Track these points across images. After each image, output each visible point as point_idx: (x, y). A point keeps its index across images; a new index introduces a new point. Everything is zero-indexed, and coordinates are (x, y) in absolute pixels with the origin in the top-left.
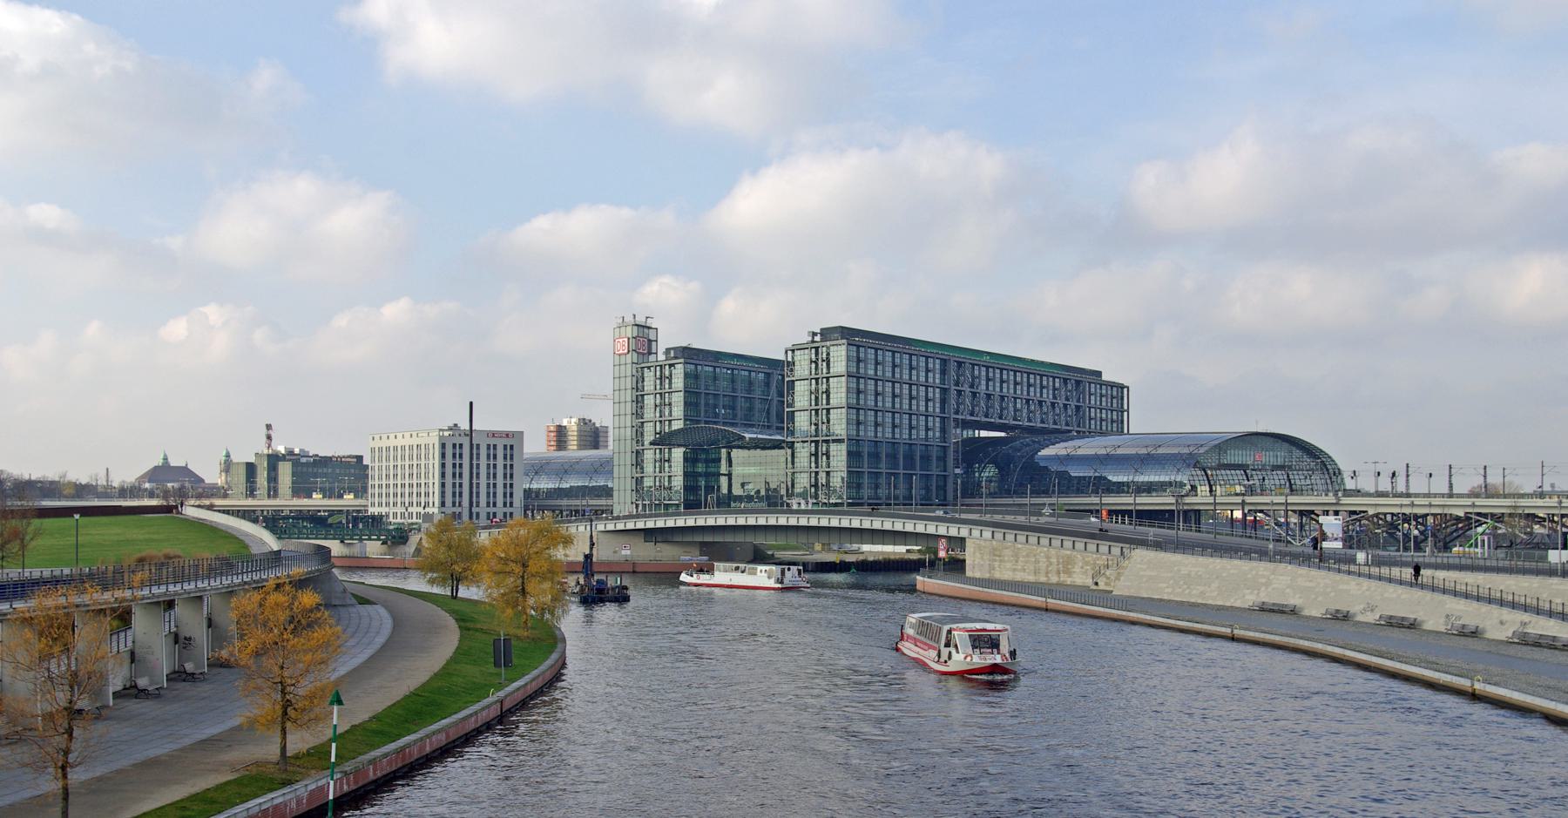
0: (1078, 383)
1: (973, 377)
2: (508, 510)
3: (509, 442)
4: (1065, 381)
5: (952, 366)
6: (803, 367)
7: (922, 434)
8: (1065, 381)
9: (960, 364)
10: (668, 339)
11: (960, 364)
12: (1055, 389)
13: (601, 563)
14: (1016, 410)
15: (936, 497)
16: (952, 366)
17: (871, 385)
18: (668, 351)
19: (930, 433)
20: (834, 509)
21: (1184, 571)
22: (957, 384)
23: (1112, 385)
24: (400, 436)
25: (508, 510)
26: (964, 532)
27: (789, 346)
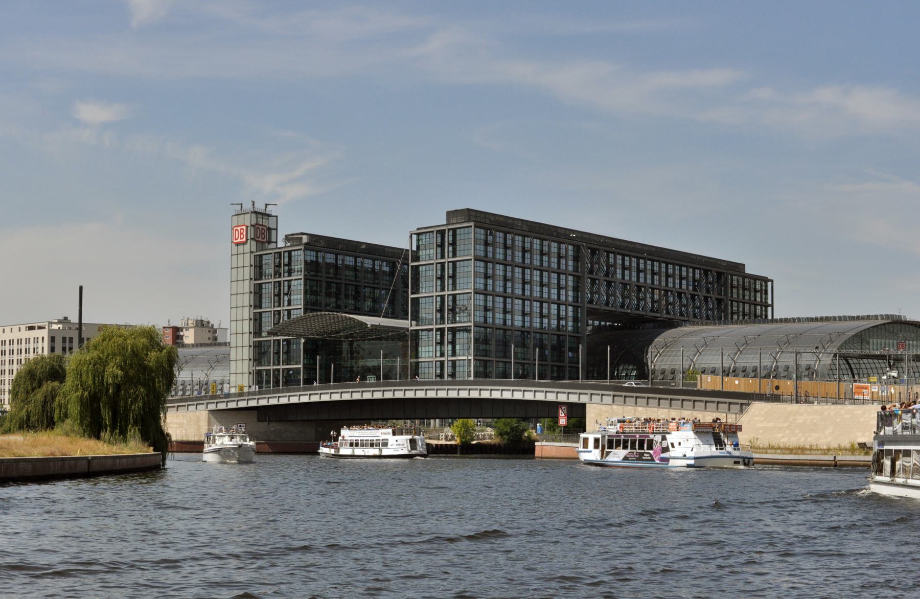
0: (719, 275)
1: (608, 266)
6: (429, 255)
8: (706, 272)
10: (287, 226)
12: (694, 280)
15: (558, 370)
17: (500, 270)
18: (288, 238)
19: (563, 323)
20: (290, 381)
21: (800, 420)
23: (755, 278)
24: (8, 329)
27: (414, 230)
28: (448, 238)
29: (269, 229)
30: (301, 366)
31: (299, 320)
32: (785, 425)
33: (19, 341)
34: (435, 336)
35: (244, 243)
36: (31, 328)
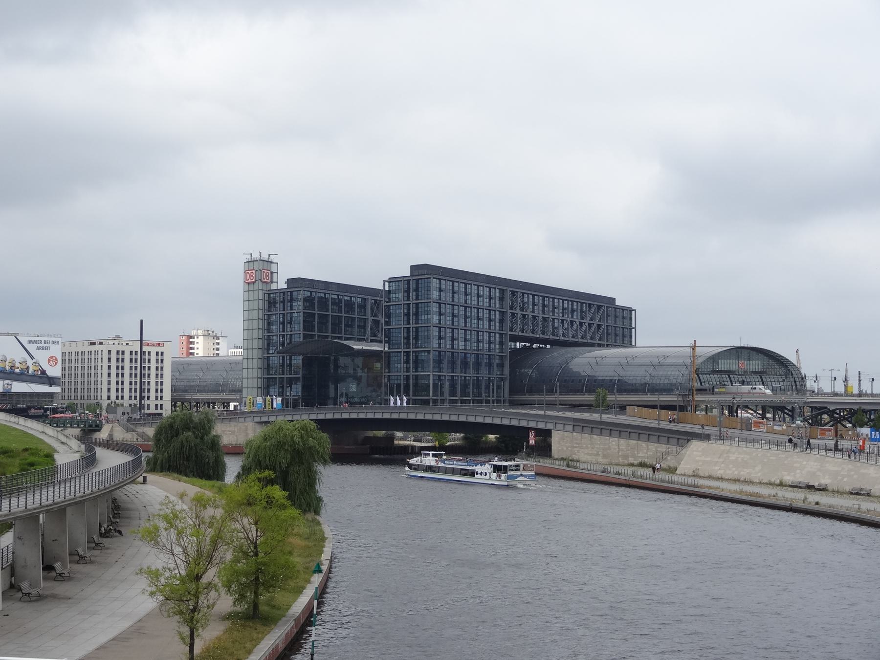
2: (159, 402)
3: (160, 349)
4: (590, 305)
5: (508, 295)
7: (486, 346)
9: (513, 293)
11: (513, 293)
12: (582, 312)
13: (226, 446)
14: (554, 328)
16: (508, 295)
19: (492, 346)
21: (733, 457)
22: (511, 308)
25: (159, 402)
26: (550, 426)
28: (413, 286)
29: (272, 273)
30: (300, 376)
31: (299, 344)
32: (721, 460)
33: (83, 353)
34: (403, 358)
35: (253, 283)
36: (93, 344)
